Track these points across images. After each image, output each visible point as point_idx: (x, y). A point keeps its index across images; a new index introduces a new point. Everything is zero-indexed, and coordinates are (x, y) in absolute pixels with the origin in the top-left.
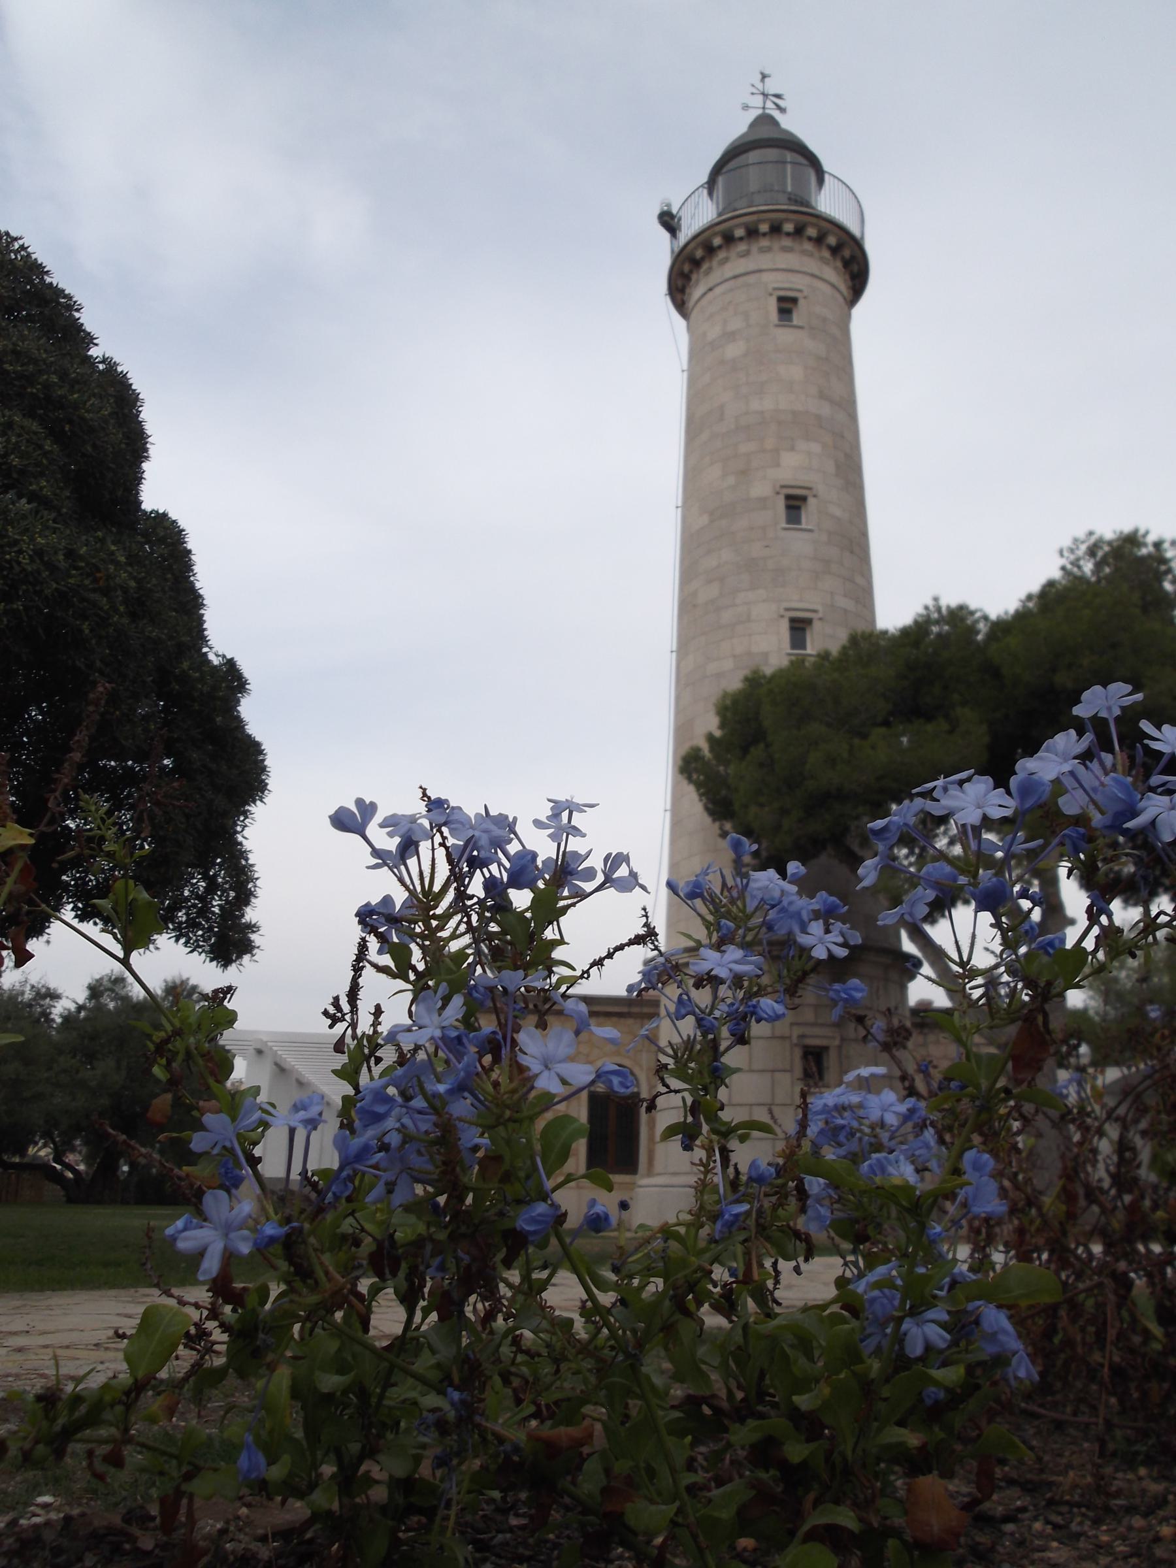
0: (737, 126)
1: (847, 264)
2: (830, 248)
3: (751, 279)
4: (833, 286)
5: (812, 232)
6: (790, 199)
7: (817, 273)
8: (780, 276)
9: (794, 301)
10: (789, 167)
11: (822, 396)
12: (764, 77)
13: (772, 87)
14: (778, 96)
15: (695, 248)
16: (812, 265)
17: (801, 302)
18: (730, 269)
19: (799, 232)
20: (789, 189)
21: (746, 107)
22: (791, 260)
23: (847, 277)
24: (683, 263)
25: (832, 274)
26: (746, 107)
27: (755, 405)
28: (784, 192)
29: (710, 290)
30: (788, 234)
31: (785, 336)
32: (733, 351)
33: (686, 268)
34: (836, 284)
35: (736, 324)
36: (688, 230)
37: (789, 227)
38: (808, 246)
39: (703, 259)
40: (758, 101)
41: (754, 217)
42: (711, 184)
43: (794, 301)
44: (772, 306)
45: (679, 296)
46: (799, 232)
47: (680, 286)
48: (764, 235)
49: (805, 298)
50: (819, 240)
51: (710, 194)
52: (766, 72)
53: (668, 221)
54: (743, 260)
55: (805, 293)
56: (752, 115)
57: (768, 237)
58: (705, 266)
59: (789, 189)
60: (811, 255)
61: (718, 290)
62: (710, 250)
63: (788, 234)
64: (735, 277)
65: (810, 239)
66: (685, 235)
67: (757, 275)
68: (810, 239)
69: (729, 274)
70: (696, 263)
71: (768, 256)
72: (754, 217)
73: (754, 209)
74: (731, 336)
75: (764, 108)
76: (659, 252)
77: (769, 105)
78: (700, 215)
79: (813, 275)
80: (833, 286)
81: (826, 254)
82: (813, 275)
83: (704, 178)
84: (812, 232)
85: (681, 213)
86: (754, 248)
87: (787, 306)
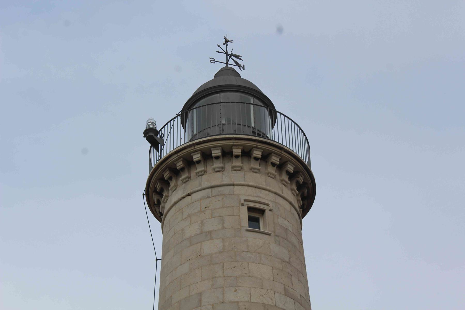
0: (206, 75)
1: (300, 187)
2: (288, 173)
3: (226, 190)
4: (291, 203)
5: (275, 159)
6: (254, 132)
7: (279, 192)
8: (250, 190)
9: (262, 212)
10: (252, 106)
11: (287, 293)
12: (227, 41)
13: (231, 48)
14: (238, 57)
15: (177, 160)
16: (275, 185)
17: (267, 213)
18: (206, 181)
19: (265, 158)
20: (253, 125)
21: (213, 61)
22: (259, 179)
23: (300, 198)
24: (164, 170)
25: (289, 193)
26: (213, 61)
27: (230, 296)
28: (249, 127)
29: (189, 195)
30: (256, 159)
31: (254, 239)
32: (210, 247)
33: (167, 175)
34: (293, 202)
35: (212, 225)
36: (168, 149)
37: (257, 153)
38: (272, 170)
39: (182, 169)
40: (223, 58)
41: (230, 142)
42: (185, 114)
43: (262, 212)
44: (245, 214)
45: (156, 198)
46: (265, 158)
47: (157, 193)
48: (237, 157)
49: (270, 210)
50: (280, 167)
51: (183, 124)
52: (229, 38)
53: (153, 136)
54: (219, 174)
55: (271, 207)
56: (218, 67)
57: (239, 159)
58: (184, 176)
59: (253, 125)
60: (274, 178)
61: (195, 197)
62: (189, 163)
63: (256, 159)
64: (211, 187)
65: (273, 164)
66: (167, 150)
67: (232, 187)
68: (273, 164)
69: (206, 184)
70: (176, 173)
71: (240, 174)
72: (230, 142)
73: (224, 136)
74: (209, 235)
75: (227, 63)
76: (139, 163)
77: (231, 62)
78: (176, 138)
79: (276, 193)
80: (291, 203)
81: (285, 177)
82: (276, 193)
83: (179, 109)
84: (275, 159)
85: (165, 131)
86: (228, 166)
87: (255, 215)
